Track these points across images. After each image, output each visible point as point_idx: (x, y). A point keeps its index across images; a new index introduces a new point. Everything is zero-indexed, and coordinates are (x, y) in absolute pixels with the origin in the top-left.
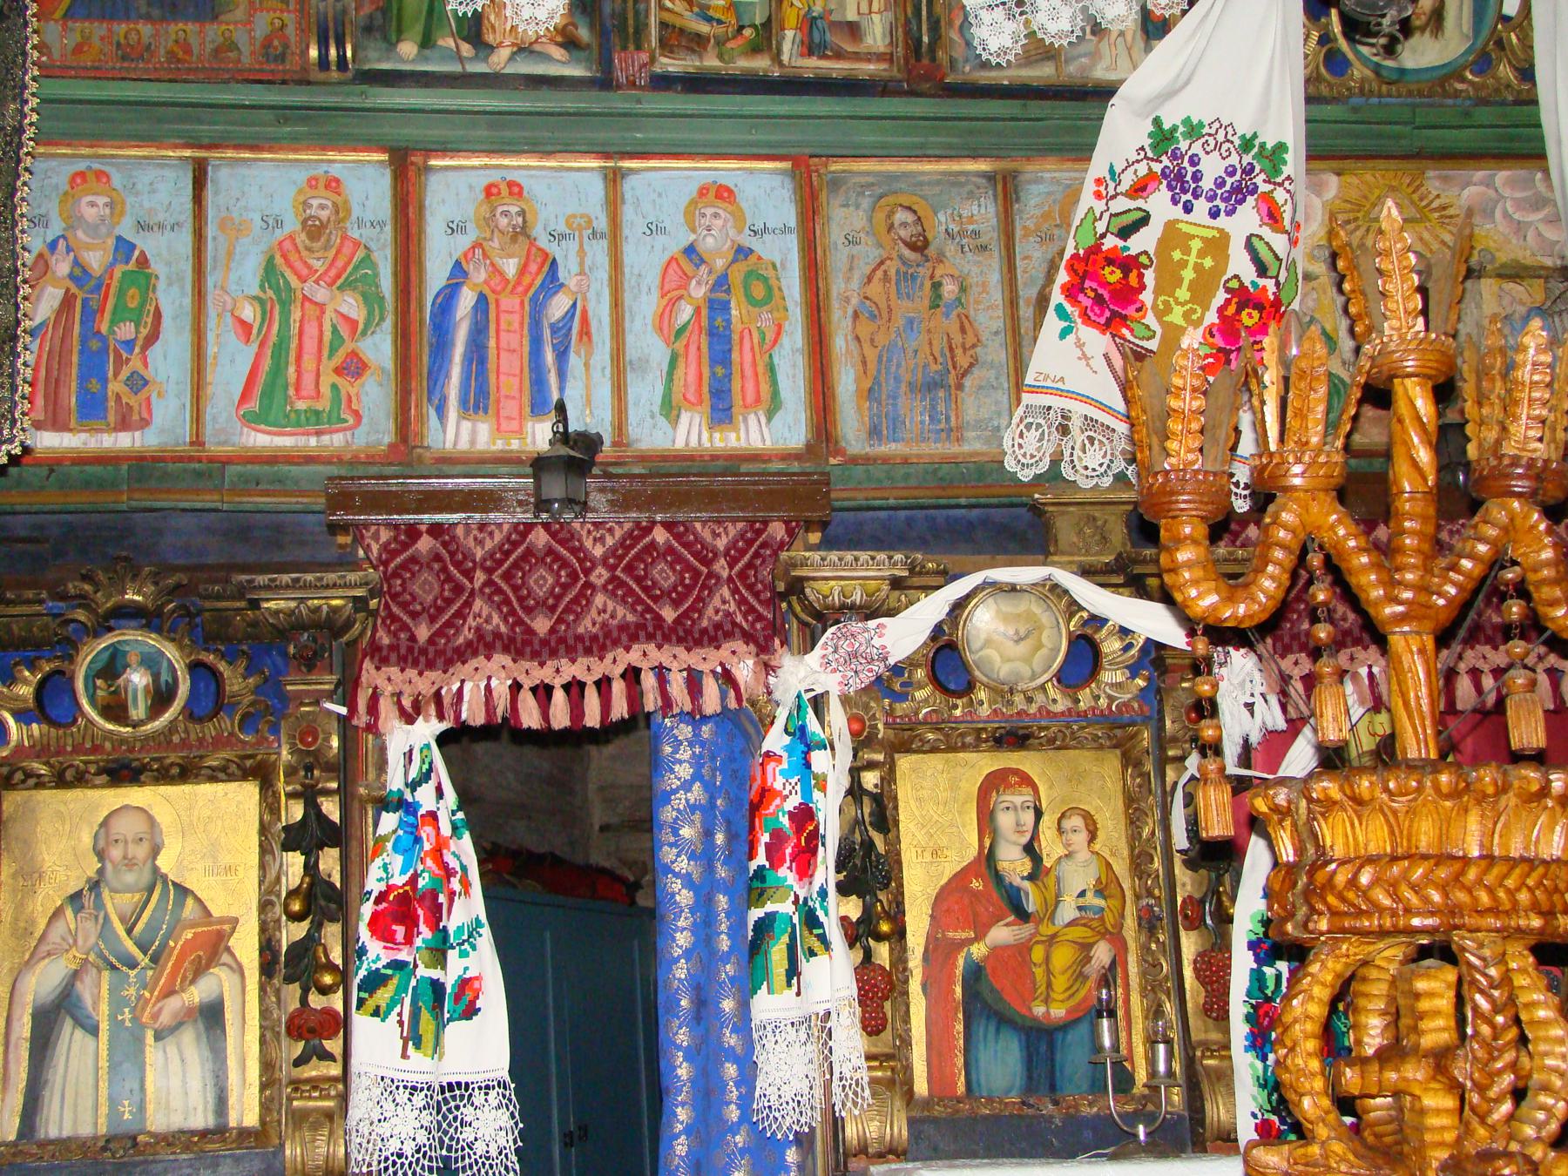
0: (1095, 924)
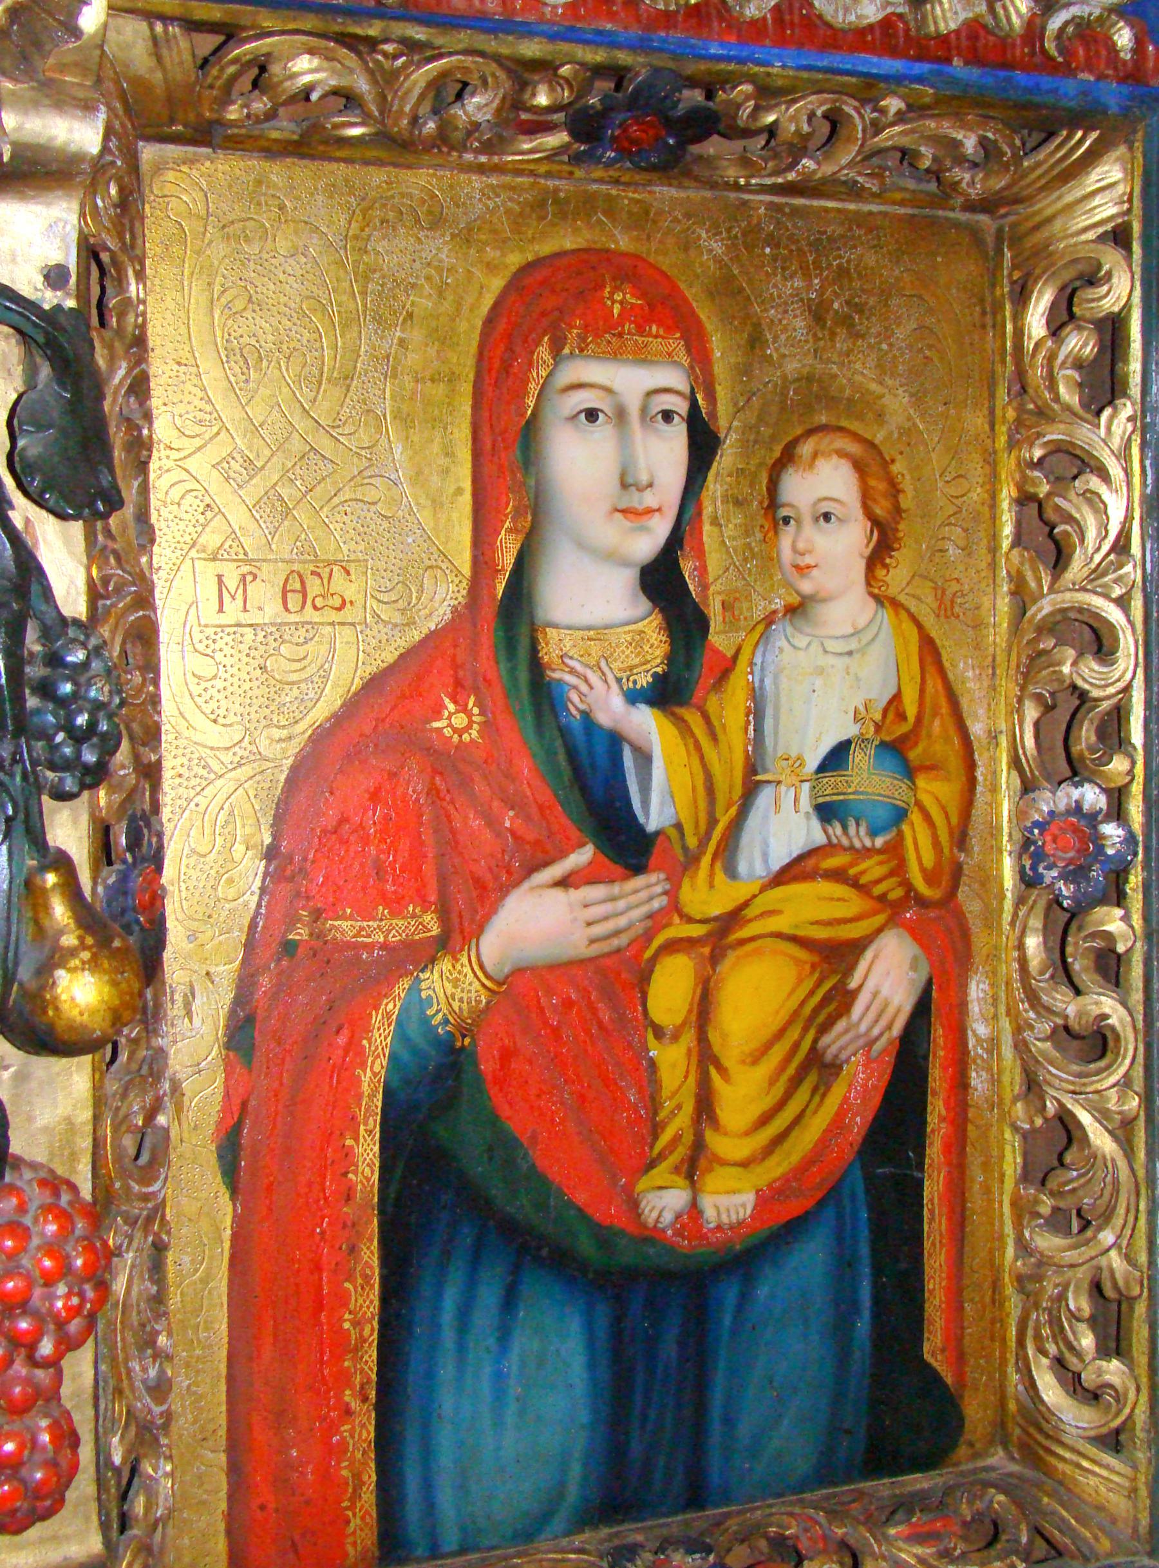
0: (872, 869)
